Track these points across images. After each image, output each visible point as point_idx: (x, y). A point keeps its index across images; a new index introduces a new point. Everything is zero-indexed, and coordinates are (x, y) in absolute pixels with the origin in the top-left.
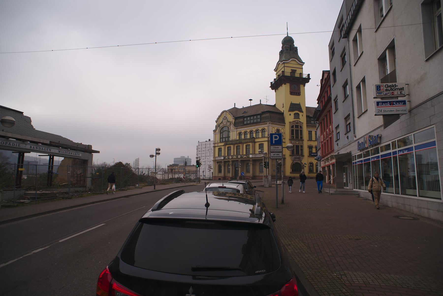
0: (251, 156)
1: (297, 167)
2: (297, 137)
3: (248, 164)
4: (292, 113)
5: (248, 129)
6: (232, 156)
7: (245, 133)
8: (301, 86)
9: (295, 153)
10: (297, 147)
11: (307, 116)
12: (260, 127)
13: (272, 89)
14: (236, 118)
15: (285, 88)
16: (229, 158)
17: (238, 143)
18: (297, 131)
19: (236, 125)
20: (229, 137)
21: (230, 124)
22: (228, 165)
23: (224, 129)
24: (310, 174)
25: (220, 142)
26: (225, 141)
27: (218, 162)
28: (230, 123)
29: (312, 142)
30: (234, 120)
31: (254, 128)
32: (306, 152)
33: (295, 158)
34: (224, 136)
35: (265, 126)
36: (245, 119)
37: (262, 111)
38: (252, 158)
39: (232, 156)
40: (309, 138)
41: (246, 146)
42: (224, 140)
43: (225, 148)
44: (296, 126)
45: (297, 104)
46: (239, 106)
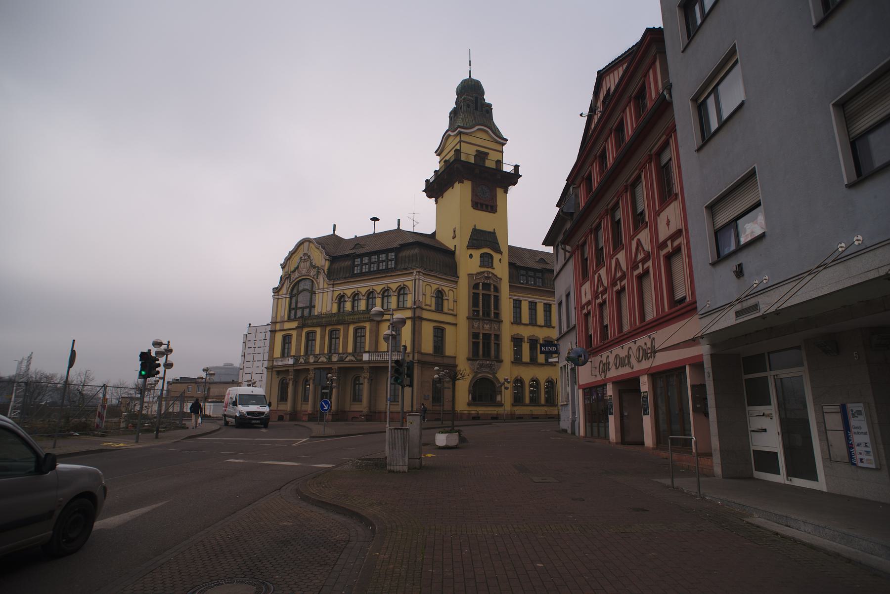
0: (366, 357)
1: (485, 390)
2: (487, 313)
3: (357, 378)
4: (477, 253)
5: (363, 287)
6: (316, 356)
7: (355, 297)
8: (499, 191)
9: (481, 352)
10: (487, 337)
11: (510, 263)
12: (393, 283)
13: (429, 196)
14: (333, 260)
15: (460, 193)
16: (307, 362)
17: (333, 323)
18: (486, 297)
19: (333, 276)
20: (312, 307)
21: (318, 272)
22: (306, 381)
23: (302, 286)
24: (516, 408)
25: (290, 320)
26: (302, 316)
27: (278, 373)
28: (318, 270)
29: (522, 327)
30: (327, 264)
31: (378, 285)
32: (507, 350)
33: (481, 366)
34: (300, 305)
35: (407, 281)
36: (358, 261)
37: (402, 242)
38: (369, 362)
39: (316, 356)
40: (515, 317)
41: (356, 330)
42: (299, 314)
43: (299, 336)
44: (484, 284)
45: (489, 233)
46: (346, 233)
